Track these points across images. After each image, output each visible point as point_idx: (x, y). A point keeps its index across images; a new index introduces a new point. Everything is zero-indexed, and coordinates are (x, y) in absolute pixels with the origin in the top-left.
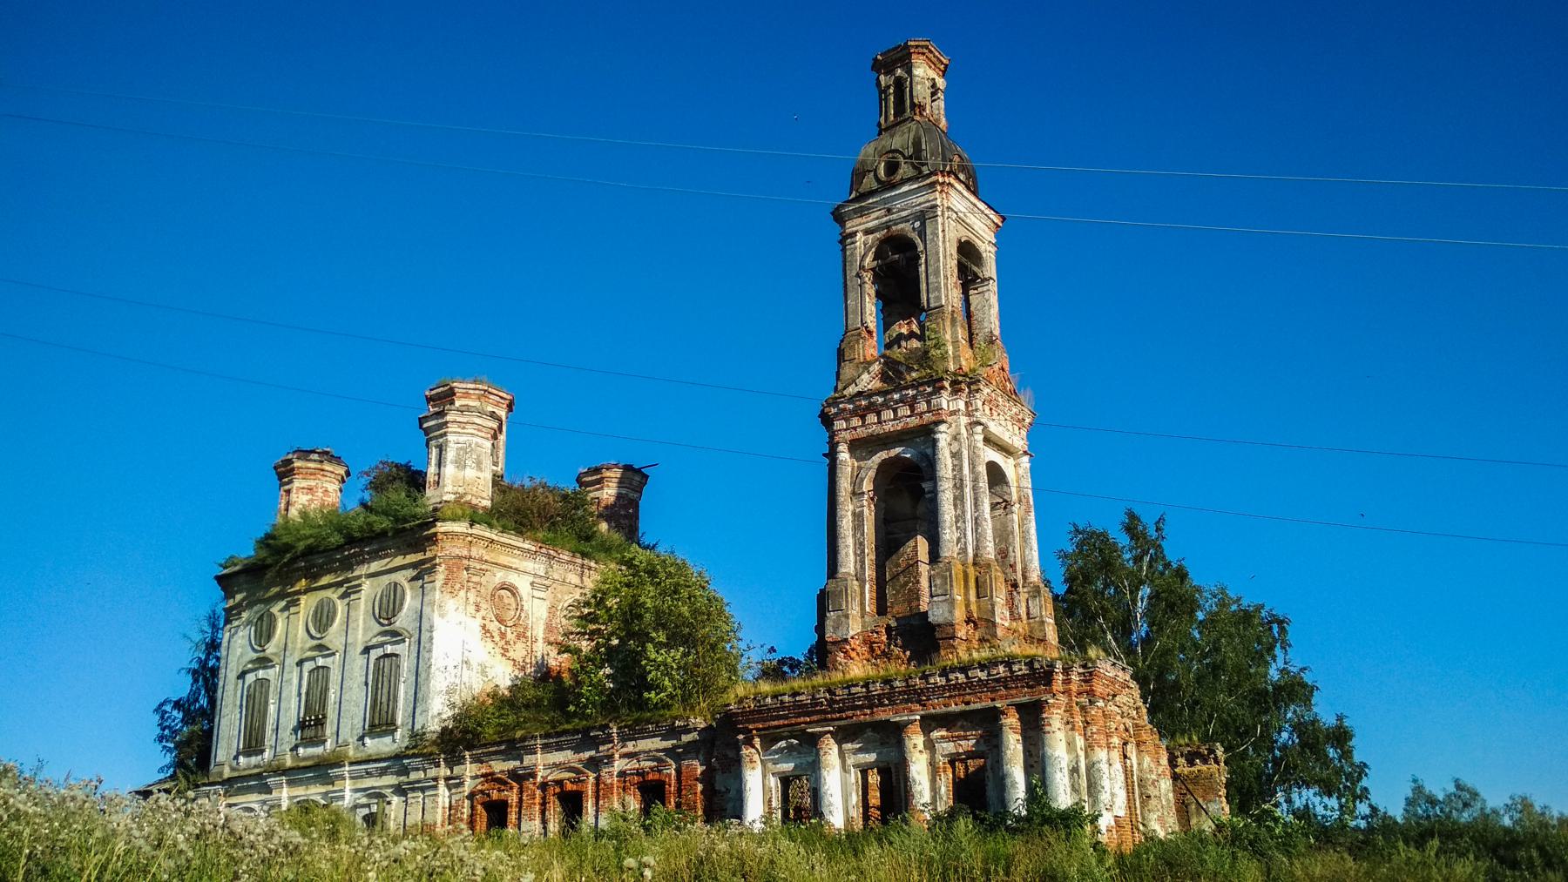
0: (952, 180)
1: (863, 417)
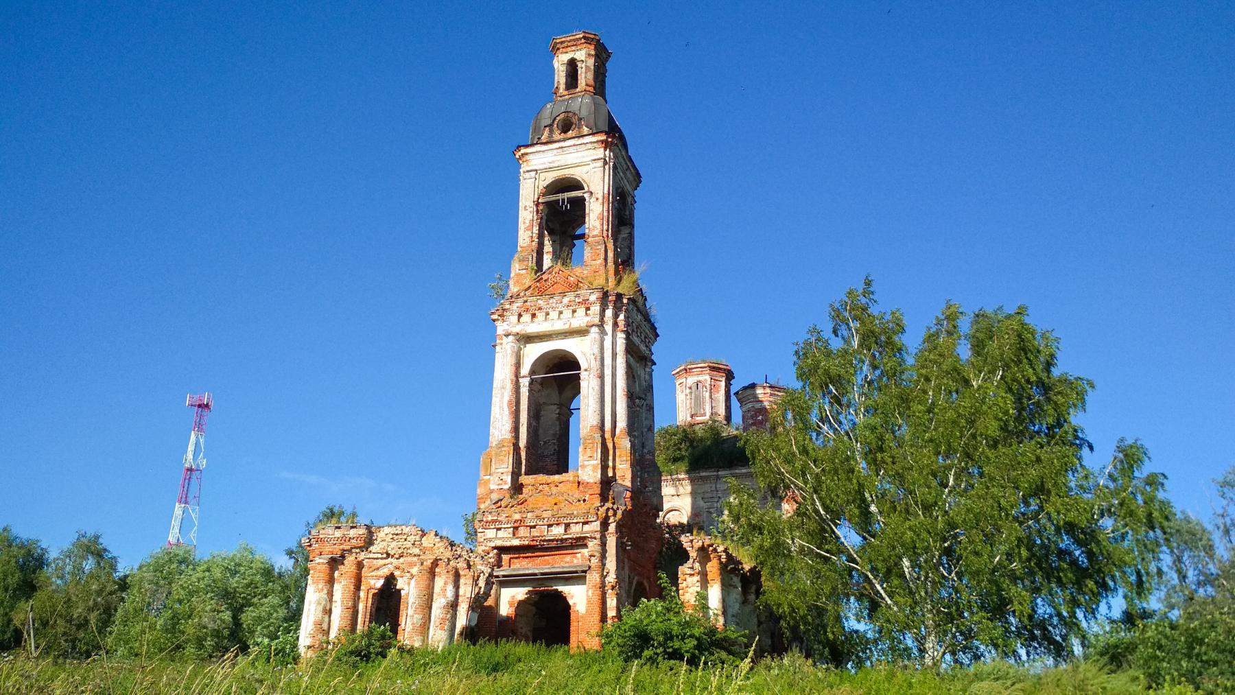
0: (523, 151)
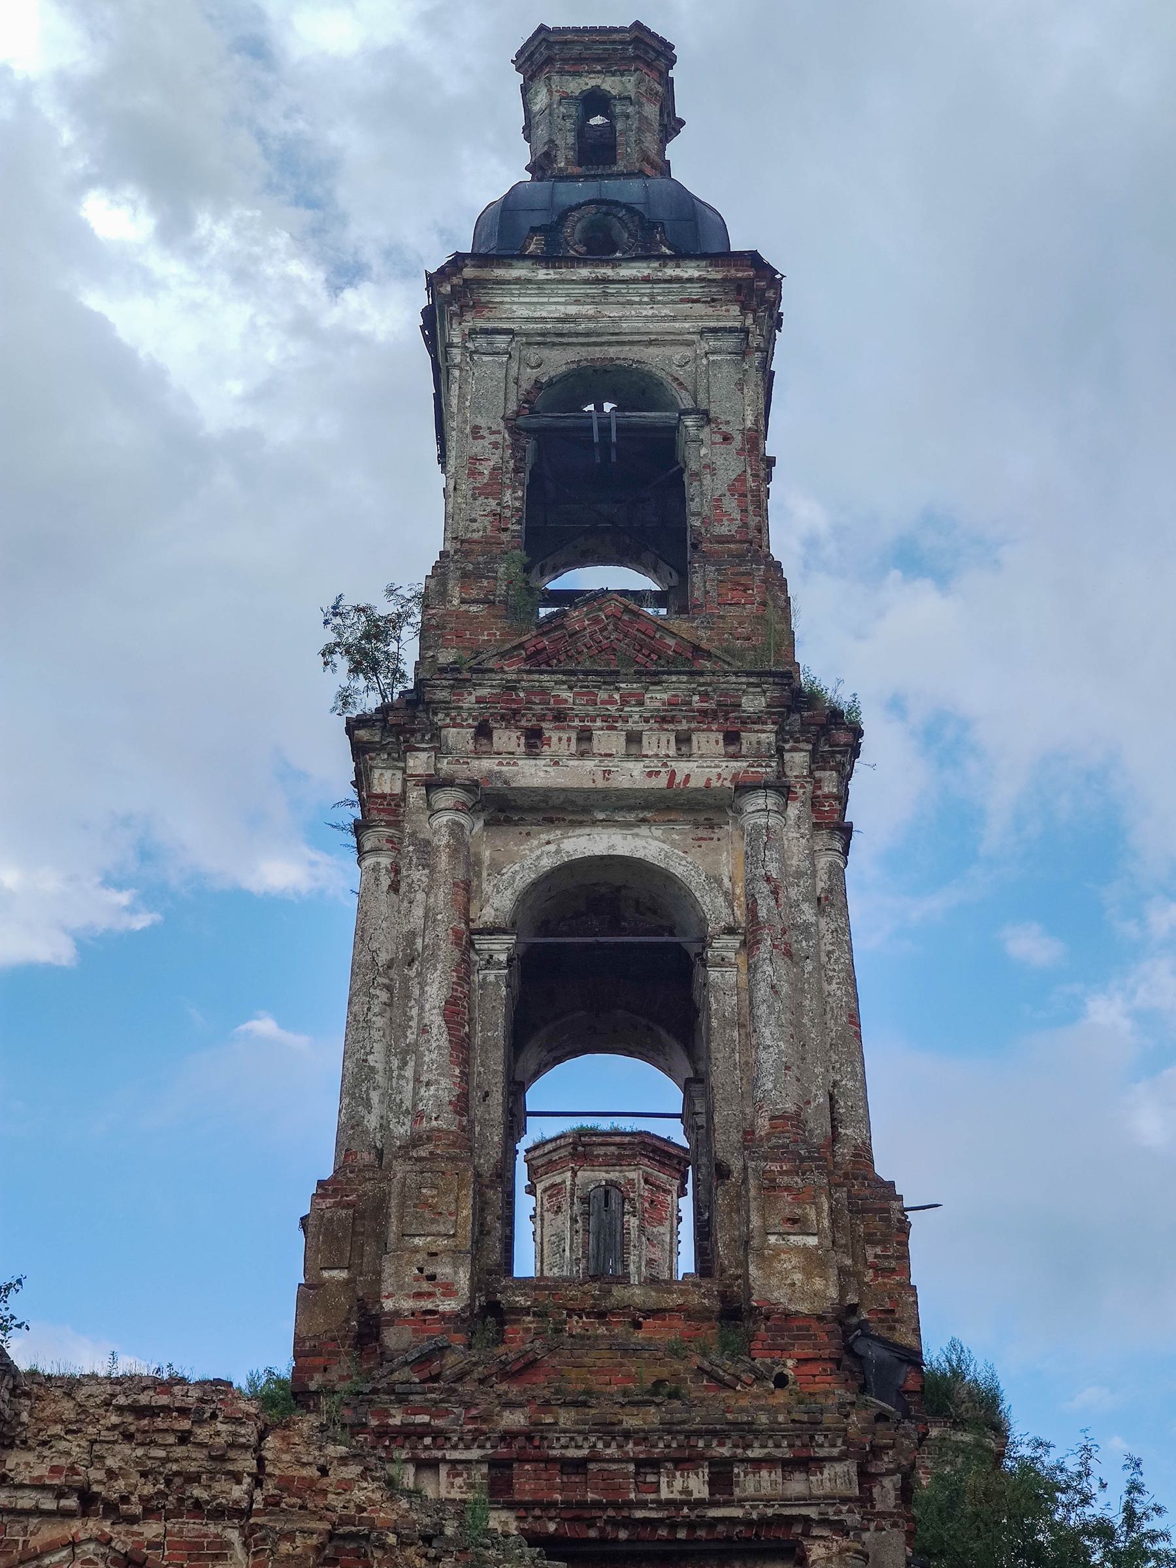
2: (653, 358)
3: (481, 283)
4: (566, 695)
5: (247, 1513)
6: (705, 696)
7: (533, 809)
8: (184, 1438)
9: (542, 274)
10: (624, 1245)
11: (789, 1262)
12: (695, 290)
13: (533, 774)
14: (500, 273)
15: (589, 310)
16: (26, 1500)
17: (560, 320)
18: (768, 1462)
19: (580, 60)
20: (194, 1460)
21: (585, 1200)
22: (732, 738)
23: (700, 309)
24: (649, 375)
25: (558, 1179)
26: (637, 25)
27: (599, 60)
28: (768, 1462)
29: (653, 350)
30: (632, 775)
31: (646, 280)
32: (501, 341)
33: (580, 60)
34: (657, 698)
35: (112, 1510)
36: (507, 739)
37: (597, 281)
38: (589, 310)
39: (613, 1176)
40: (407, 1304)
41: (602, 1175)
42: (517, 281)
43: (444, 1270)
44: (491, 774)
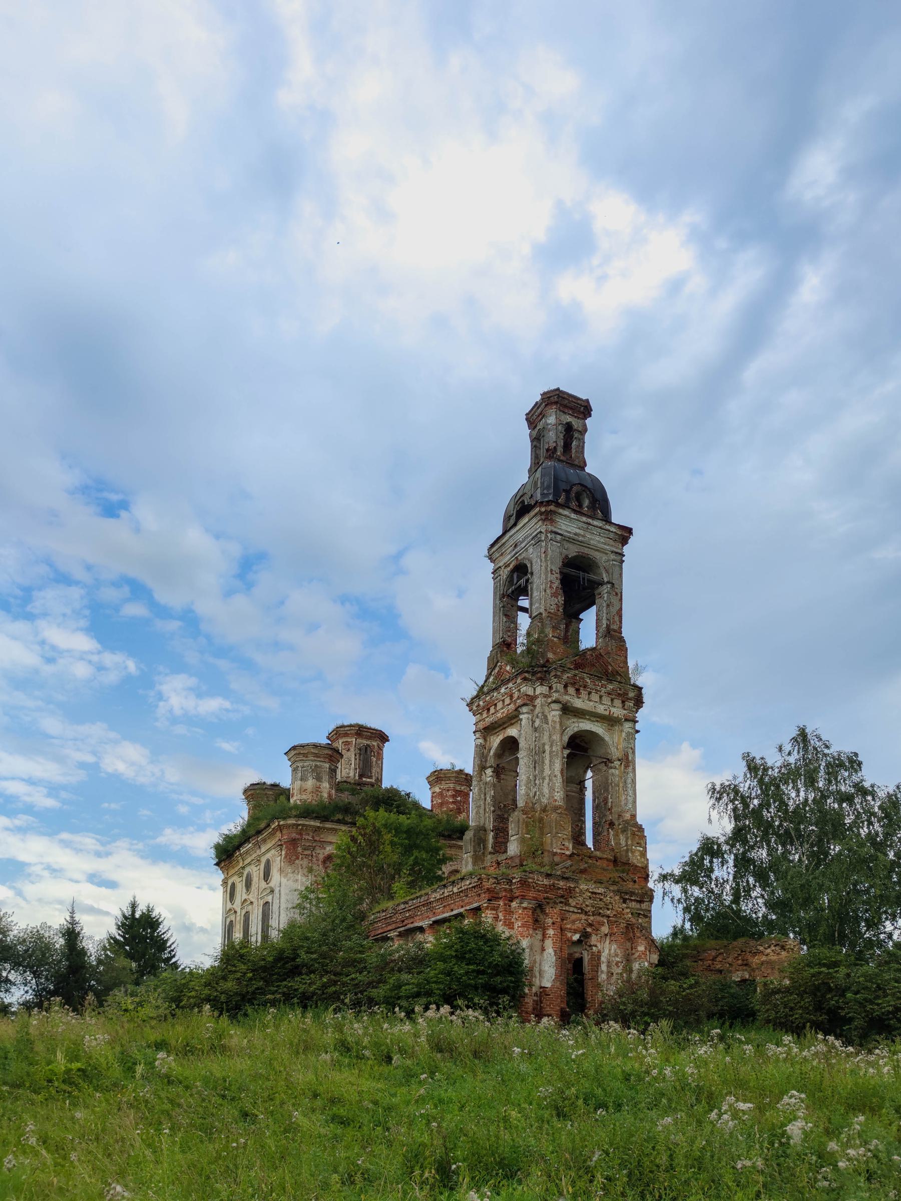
1: (488, 710)
2: (597, 555)
3: (555, 512)
4: (588, 681)
5: (609, 917)
6: (620, 689)
7: (572, 711)
8: (601, 900)
9: (573, 516)
10: (371, 766)
11: (637, 854)
12: (612, 535)
13: (578, 703)
14: (561, 511)
15: (582, 532)
16: (572, 909)
17: (575, 534)
18: (634, 900)
19: (565, 406)
20: (601, 904)
21: (360, 749)
22: (623, 702)
23: (611, 542)
24: (594, 562)
25: (349, 740)
26: (587, 401)
27: (571, 408)
28: (634, 900)
29: (597, 553)
30: (601, 709)
31: (600, 528)
32: (559, 538)
33: (565, 406)
34: (610, 687)
35: (586, 913)
36: (571, 690)
37: (587, 523)
38: (582, 532)
39: (368, 742)
40: (559, 851)
41: (365, 742)
42: (565, 516)
43: (567, 844)
44: (568, 701)
